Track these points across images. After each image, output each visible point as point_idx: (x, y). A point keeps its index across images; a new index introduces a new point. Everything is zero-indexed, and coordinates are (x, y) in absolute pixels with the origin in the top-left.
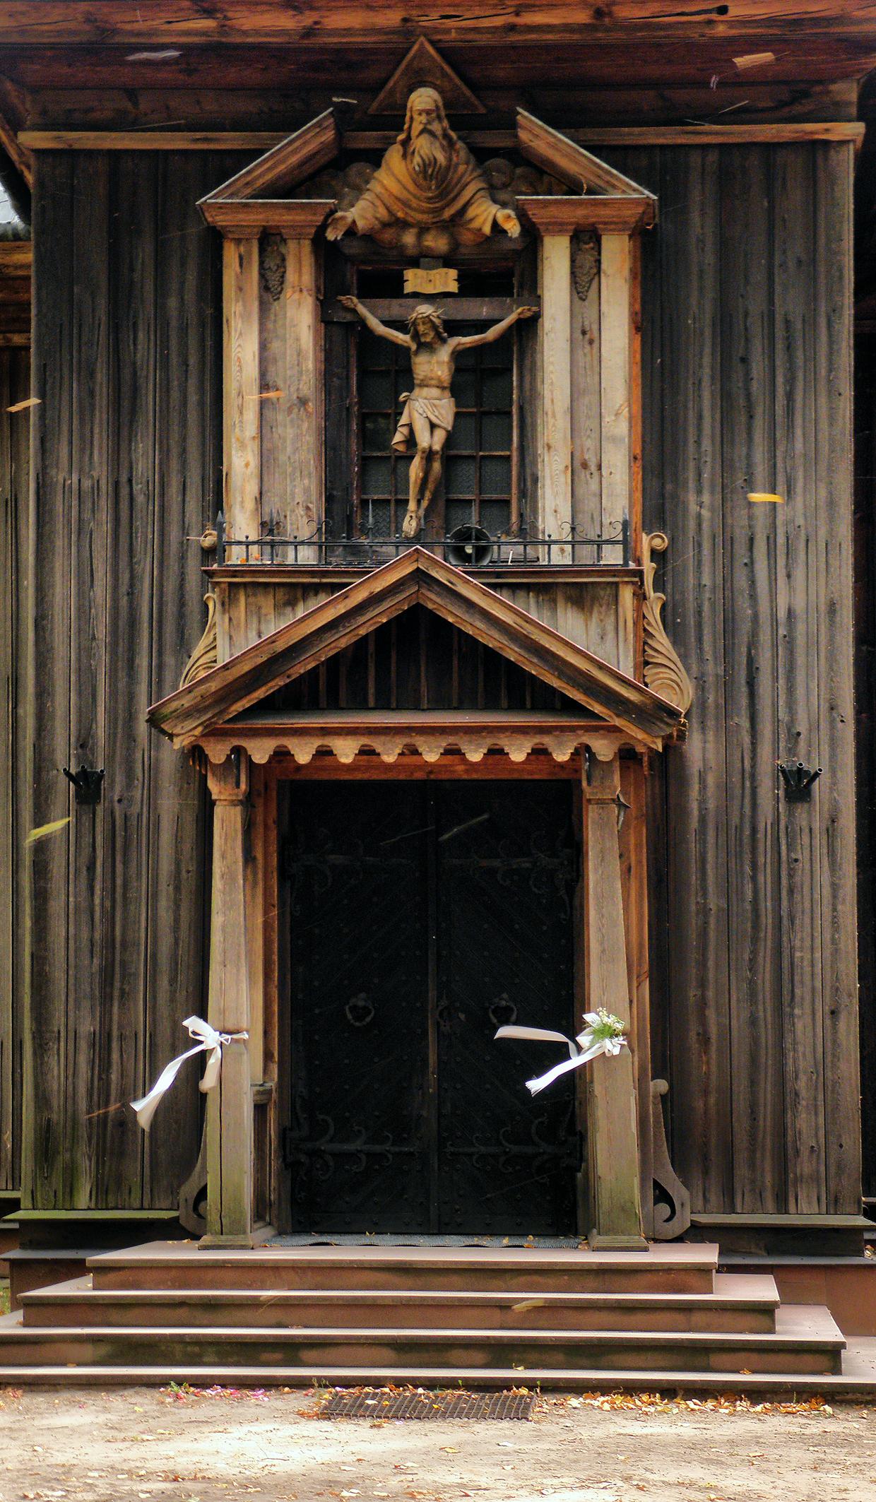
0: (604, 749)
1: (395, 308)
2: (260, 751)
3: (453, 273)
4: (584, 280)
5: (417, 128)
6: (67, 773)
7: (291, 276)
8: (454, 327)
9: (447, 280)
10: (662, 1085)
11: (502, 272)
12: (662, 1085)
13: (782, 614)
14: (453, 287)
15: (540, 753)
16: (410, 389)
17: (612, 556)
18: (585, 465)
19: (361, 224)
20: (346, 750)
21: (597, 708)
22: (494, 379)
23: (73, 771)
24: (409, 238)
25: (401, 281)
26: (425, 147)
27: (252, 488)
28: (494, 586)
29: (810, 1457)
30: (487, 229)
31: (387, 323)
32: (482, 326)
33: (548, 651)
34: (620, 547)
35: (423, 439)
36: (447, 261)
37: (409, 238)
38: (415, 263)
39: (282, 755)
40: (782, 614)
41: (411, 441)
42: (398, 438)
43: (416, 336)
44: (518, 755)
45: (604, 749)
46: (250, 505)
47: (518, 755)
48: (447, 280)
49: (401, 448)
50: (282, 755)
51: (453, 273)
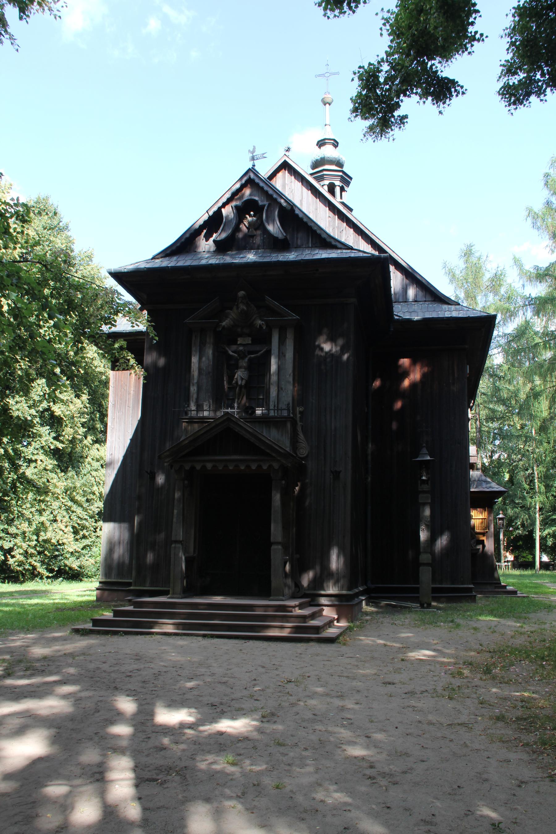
0: (276, 465)
1: (234, 347)
2: (187, 467)
3: (250, 338)
4: (282, 342)
5: (240, 301)
6: (147, 472)
7: (208, 340)
8: (251, 353)
9: (248, 340)
10: (298, 556)
11: (263, 338)
12: (298, 556)
13: (333, 428)
14: (250, 342)
15: (259, 467)
16: (237, 369)
17: (285, 413)
18: (282, 389)
19: (226, 326)
20: (209, 466)
21: (274, 455)
22: (259, 367)
23: (149, 472)
24: (239, 330)
25: (237, 341)
26: (243, 307)
27: (195, 396)
28: (247, 422)
29: (186, 696)
30: (258, 327)
31: (232, 352)
32: (257, 352)
33: (261, 439)
34: (286, 411)
35: (239, 383)
36: (249, 335)
37: (239, 330)
38: (241, 336)
39: (193, 468)
40: (333, 428)
41: (237, 382)
42: (234, 382)
43: (239, 355)
44: (254, 467)
45: (276, 465)
46: (194, 400)
47: (254, 467)
48: (248, 340)
49: (235, 385)
50: (204, 467)
51: (250, 338)
